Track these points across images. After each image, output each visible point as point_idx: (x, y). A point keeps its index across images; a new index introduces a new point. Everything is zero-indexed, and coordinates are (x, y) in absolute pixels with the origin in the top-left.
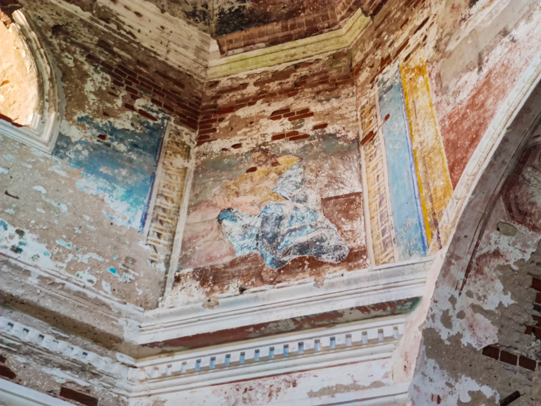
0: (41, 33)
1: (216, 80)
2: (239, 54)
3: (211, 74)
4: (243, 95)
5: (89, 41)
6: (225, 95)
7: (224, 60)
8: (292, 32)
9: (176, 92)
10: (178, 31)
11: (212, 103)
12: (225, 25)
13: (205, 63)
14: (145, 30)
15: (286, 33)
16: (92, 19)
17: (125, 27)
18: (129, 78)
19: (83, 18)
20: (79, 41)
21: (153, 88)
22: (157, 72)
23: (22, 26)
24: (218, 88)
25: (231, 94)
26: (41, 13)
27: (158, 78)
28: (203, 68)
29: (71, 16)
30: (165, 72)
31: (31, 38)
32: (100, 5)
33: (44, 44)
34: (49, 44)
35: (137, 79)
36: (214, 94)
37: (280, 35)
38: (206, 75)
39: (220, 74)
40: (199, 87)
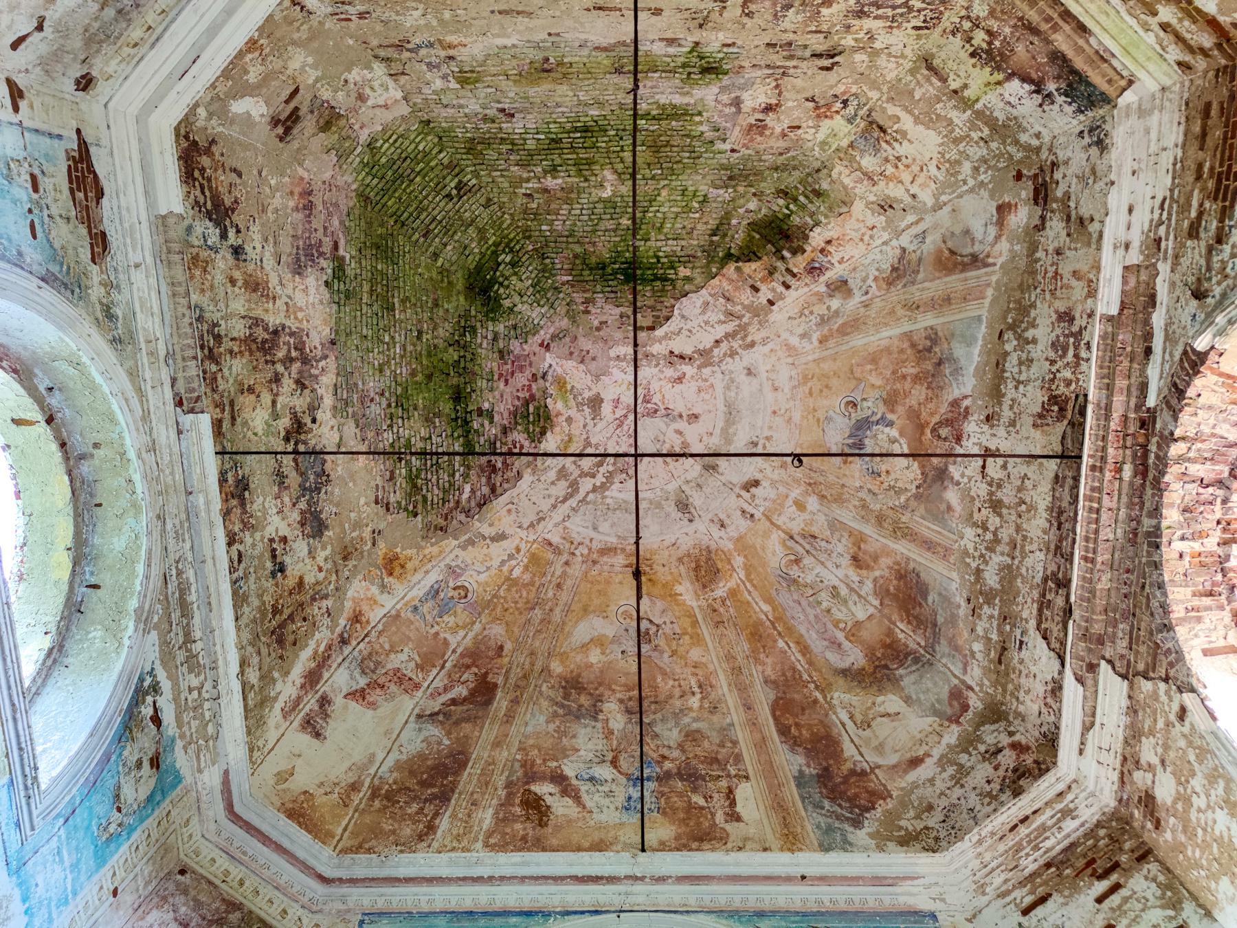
0: (1213, 311)
1: (1176, 67)
2: (1123, 61)
3: (1168, 75)
4: (1180, 20)
5: (1196, 251)
6: (1192, 43)
7: (1140, 74)
8: (1055, 16)
9: (1222, 108)
10: (1129, 151)
11: (1216, 52)
12: (1094, 98)
13: (1158, 95)
14: (1149, 192)
15: (1061, 23)
16: (1165, 258)
17: (1156, 216)
18: (1228, 179)
19: (1169, 269)
20: (1203, 262)
21: (1230, 141)
22: (1201, 149)
23: (1215, 336)
24: (1188, 58)
25: (1188, 36)
26: (1186, 319)
27: (1210, 143)
28: (1167, 93)
29: (1173, 285)
30: (1196, 138)
31: (1226, 319)
32: (1141, 258)
33: (1227, 302)
34: (1224, 296)
35: (1225, 168)
36: (1199, 57)
37: (1067, 28)
38: (1175, 84)
39: (1165, 66)
40: (1200, 82)
